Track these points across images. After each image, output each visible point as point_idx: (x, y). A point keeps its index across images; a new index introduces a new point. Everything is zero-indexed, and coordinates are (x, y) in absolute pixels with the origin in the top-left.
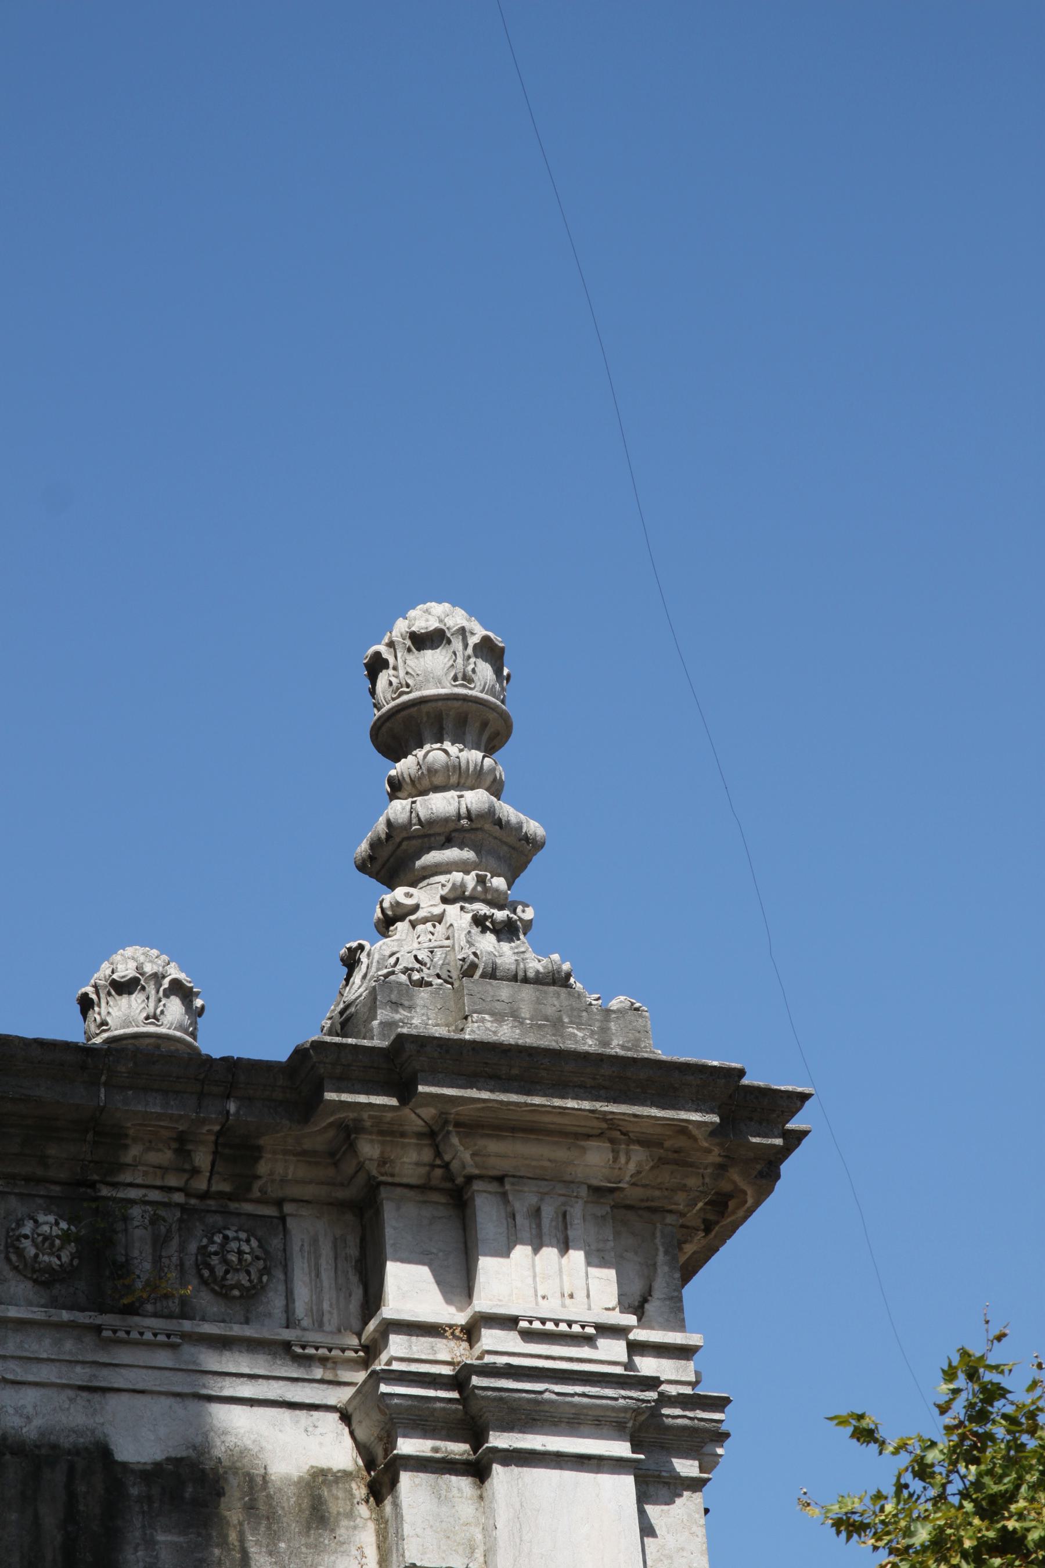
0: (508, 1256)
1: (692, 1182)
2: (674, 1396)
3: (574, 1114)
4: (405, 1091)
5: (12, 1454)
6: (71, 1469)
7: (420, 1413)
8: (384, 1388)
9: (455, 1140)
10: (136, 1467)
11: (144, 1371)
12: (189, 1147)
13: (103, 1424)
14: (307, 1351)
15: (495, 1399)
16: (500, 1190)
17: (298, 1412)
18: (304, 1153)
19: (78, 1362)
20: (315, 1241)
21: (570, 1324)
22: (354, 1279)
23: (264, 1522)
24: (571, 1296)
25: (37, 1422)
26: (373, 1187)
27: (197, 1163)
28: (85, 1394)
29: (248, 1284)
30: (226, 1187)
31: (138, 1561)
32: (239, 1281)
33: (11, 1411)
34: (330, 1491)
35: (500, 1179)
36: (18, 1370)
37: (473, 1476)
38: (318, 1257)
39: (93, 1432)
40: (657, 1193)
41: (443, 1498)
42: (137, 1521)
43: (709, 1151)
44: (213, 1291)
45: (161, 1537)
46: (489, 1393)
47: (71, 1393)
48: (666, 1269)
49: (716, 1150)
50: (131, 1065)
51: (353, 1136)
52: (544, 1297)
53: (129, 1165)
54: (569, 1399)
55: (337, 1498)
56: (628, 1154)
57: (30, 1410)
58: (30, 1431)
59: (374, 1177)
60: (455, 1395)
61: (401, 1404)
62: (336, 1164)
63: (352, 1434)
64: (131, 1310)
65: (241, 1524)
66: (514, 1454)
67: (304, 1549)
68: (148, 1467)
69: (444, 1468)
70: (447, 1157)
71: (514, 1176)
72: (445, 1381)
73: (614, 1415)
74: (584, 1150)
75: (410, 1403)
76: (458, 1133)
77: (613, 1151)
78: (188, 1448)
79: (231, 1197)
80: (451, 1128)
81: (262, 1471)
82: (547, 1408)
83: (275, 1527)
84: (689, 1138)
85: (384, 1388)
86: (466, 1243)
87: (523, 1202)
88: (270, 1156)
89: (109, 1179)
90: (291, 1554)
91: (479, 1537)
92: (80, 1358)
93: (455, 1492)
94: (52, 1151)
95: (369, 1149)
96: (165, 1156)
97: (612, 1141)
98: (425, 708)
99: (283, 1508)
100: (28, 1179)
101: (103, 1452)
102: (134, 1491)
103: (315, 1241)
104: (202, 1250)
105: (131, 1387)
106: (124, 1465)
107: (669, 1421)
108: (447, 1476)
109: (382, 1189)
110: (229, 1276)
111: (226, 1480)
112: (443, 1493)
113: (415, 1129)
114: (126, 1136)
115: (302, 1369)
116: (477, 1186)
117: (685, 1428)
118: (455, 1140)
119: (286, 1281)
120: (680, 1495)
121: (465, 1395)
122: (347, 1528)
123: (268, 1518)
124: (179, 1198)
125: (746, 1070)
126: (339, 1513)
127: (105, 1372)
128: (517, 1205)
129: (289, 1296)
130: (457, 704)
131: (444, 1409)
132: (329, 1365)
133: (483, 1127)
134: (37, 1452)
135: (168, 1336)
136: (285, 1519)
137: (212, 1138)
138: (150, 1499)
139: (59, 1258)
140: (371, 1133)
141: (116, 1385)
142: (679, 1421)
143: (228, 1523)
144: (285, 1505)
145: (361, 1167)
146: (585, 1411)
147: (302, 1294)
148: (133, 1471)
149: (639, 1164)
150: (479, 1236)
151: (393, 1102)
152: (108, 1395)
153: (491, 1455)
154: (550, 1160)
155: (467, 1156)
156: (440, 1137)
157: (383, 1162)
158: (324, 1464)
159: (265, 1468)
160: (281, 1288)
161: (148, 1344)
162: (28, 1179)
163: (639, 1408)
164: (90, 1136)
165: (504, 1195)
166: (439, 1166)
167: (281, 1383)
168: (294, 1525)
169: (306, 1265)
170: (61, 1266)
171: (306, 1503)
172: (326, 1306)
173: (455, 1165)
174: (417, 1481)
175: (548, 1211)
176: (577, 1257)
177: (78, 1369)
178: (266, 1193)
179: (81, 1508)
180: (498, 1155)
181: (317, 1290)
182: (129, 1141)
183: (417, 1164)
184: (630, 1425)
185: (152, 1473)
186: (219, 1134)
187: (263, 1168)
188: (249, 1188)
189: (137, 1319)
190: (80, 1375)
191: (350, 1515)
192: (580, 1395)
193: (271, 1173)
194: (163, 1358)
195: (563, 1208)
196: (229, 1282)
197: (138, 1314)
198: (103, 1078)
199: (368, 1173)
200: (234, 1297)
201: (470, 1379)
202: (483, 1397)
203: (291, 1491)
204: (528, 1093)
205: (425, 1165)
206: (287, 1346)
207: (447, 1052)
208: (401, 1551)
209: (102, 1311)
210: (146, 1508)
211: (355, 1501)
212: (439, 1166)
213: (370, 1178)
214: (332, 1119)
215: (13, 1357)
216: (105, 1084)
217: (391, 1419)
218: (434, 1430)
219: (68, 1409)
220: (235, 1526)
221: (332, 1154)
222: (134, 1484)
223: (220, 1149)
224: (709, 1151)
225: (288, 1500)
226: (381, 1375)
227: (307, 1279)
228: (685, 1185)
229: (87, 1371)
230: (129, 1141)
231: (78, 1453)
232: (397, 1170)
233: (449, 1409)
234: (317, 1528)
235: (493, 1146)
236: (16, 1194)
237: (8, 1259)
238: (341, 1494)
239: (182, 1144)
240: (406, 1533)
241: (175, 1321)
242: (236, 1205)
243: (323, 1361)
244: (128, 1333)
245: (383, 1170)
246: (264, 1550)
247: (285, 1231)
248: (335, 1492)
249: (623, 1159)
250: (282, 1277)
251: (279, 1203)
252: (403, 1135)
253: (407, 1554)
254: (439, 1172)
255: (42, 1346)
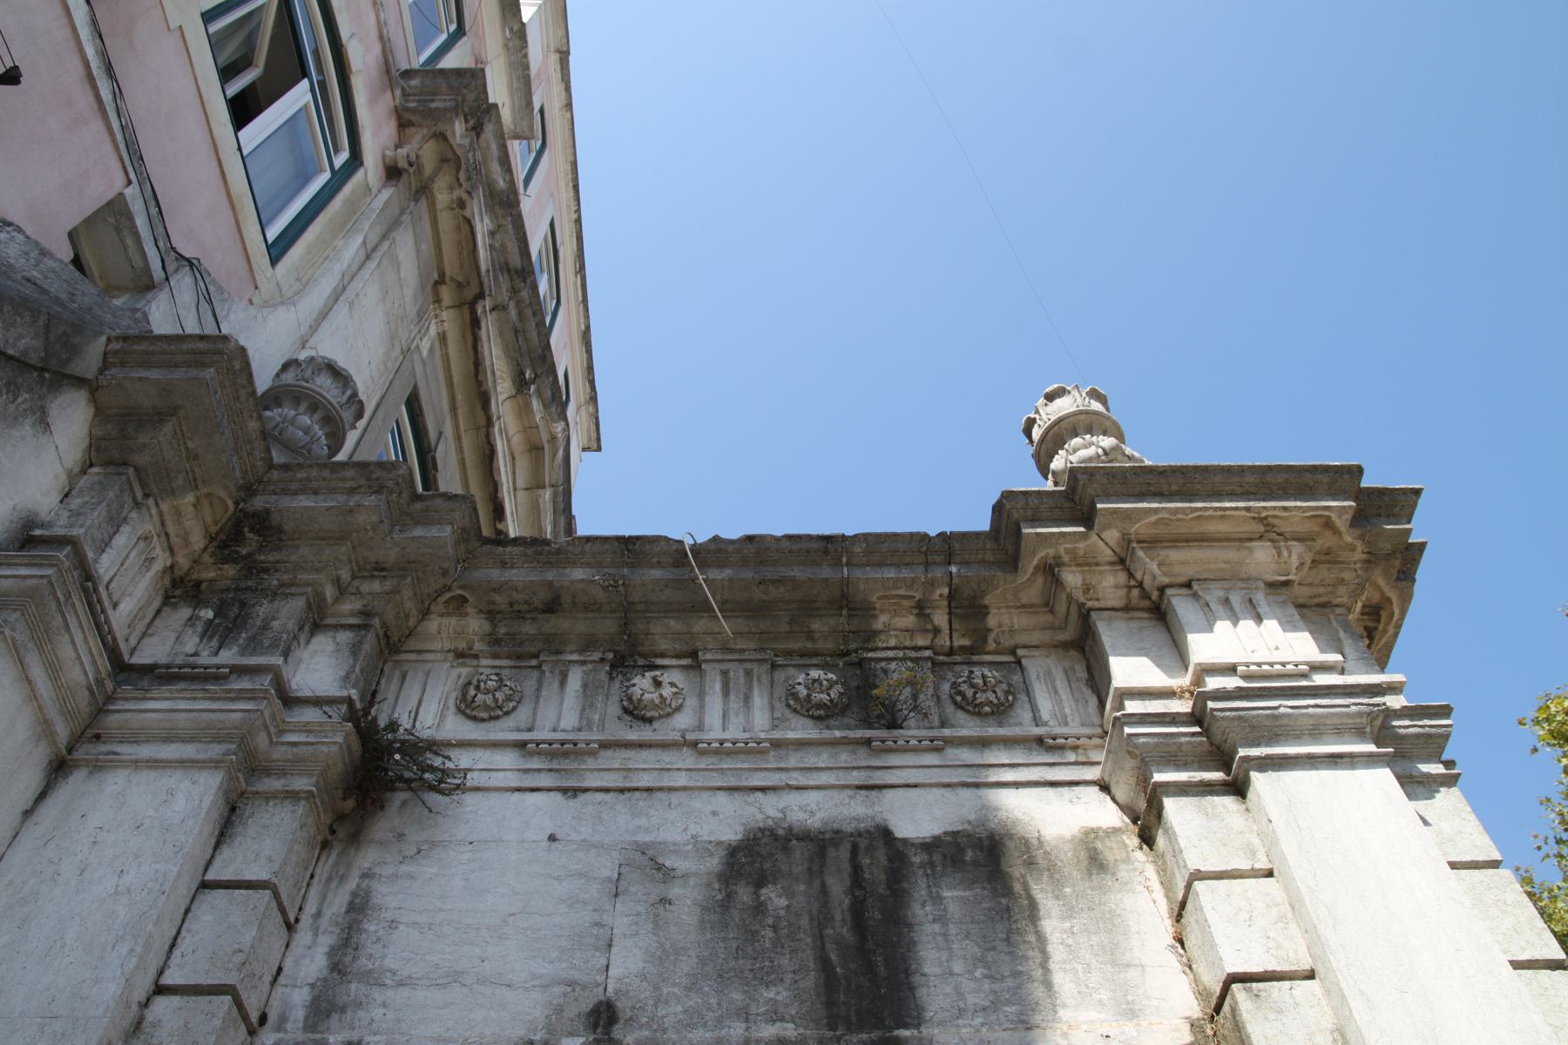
0: (1211, 631)
1: (1347, 575)
2: (1399, 710)
3: (1233, 516)
4: (1087, 518)
5: (798, 840)
6: (855, 849)
7: (1169, 749)
8: (1127, 730)
9: (1140, 553)
10: (916, 841)
11: (914, 770)
12: (927, 611)
13: (881, 812)
14: (1057, 741)
15: (1234, 718)
16: (1190, 592)
17: (1060, 789)
18: (1023, 606)
19: (854, 768)
20: (1049, 673)
21: (1283, 664)
22: (1088, 692)
23: (1046, 874)
24: (1277, 648)
25: (820, 815)
26: (1085, 616)
27: (936, 623)
28: (863, 792)
29: (995, 701)
30: (966, 642)
31: (927, 915)
32: (987, 698)
33: (796, 808)
34: (1103, 844)
35: (1188, 585)
36: (801, 778)
37: (1234, 795)
38: (1053, 681)
39: (873, 818)
40: (1322, 590)
41: (1210, 814)
42: (922, 882)
43: (1353, 549)
44: (968, 712)
45: (947, 894)
46: (1228, 714)
47: (850, 792)
48: (1350, 641)
49: (1360, 546)
50: (864, 545)
51: (1056, 569)
52: (1253, 652)
53: (881, 631)
54: (1304, 711)
55: (1112, 849)
56: (1288, 548)
57: (814, 807)
58: (815, 823)
59: (1083, 604)
60: (1197, 729)
61: (1148, 743)
62: (1051, 611)
63: (1113, 799)
64: (894, 725)
65: (1023, 876)
66: (1268, 761)
67: (1089, 892)
68: (928, 840)
69: (1203, 791)
70: (1139, 576)
71: (1198, 580)
72: (1185, 719)
73: (1351, 721)
74: (1251, 550)
75: (1156, 740)
76: (1141, 548)
77: (1275, 547)
78: (963, 824)
79: (972, 650)
80: (1134, 545)
81: (1037, 835)
82: (1285, 722)
83: (1058, 876)
84: (1335, 533)
85: (1127, 730)
86: (1174, 641)
87: (1213, 595)
88: (996, 611)
89: (866, 645)
90: (1077, 896)
91: (1256, 842)
92: (855, 764)
93: (1220, 809)
94: (816, 625)
95: (1072, 579)
96: (909, 621)
97: (1272, 541)
98: (1063, 424)
99: (1062, 861)
100: (802, 654)
101: (886, 833)
102: (917, 860)
103: (1049, 673)
104: (954, 685)
105: (904, 782)
106: (905, 841)
107: (1402, 731)
108: (1209, 797)
109: (1092, 613)
110: (978, 696)
111: (1003, 844)
112: (1210, 811)
113: (1106, 559)
114: (875, 609)
115: (1057, 756)
116: (1169, 592)
117: (1418, 736)
118: (1140, 553)
119: (1030, 701)
120: (1438, 791)
121: (1206, 725)
122: (1127, 871)
123: (1049, 870)
124: (927, 653)
125: (1363, 466)
126: (1116, 860)
127: (879, 773)
128: (1208, 598)
129: (1034, 709)
130: (1083, 417)
131: (1189, 742)
132: (1080, 751)
133: (1161, 541)
134: (821, 837)
135: (932, 741)
136: (1066, 870)
137: (946, 603)
138: (932, 865)
139: (829, 695)
140: (1071, 566)
141: (890, 782)
142: (1412, 730)
143: (1011, 877)
144: (1064, 858)
145: (1070, 597)
146: (1322, 720)
147: (1045, 706)
148: (913, 844)
149: (1300, 556)
150: (1183, 622)
151: (1082, 529)
152: (884, 791)
153: (1245, 765)
154: (1225, 562)
155: (1154, 567)
156: (1128, 560)
157: (1087, 589)
158: (1094, 824)
159: (1039, 832)
160: (1027, 706)
161: (915, 750)
162: (802, 654)
163: (1372, 712)
164: (845, 612)
165: (1195, 596)
166: (1134, 587)
167: (1040, 768)
168: (1075, 874)
169: (1044, 687)
170: (831, 701)
171: (1083, 854)
172: (1067, 711)
173: (1147, 583)
174: (1181, 803)
175: (1236, 599)
176: (1271, 625)
177: (855, 773)
178: (999, 643)
179: (867, 876)
180: (1181, 563)
181: (1057, 701)
182: (877, 612)
183: (1116, 587)
184: (1368, 729)
185: (930, 846)
186: (950, 597)
187: (992, 621)
188: (985, 641)
189: (901, 731)
190: (857, 777)
191: (1127, 860)
192: (1313, 706)
193: (1000, 626)
194: (930, 759)
195: (1248, 596)
196: (978, 701)
197: (902, 728)
198: (844, 560)
199: (1077, 601)
200: (987, 714)
201: (1206, 705)
202: (1222, 717)
203: (1067, 847)
204: (1190, 501)
205: (1122, 587)
206: (1040, 741)
207: (1114, 477)
208: (1182, 864)
209: (870, 727)
210: (929, 872)
211: (1130, 849)
212: (1134, 587)
213: (1081, 606)
214: (1035, 562)
215: (795, 769)
216: (847, 565)
217: (1143, 760)
218: (1186, 764)
219: (849, 804)
220: (1018, 879)
221: (1047, 605)
222: (916, 854)
223: (953, 610)
224: (1353, 549)
225: (1065, 853)
226: (1123, 720)
227: (1047, 695)
228: (1343, 579)
229: (863, 773)
230: (877, 612)
231: (860, 835)
232: (1100, 595)
233: (1194, 742)
234: (1098, 874)
235: (1174, 555)
236: (794, 666)
237: (788, 706)
238: (1114, 845)
239: (921, 609)
240: (1182, 845)
241: (935, 730)
242: (978, 657)
243: (1075, 748)
244: (895, 742)
245: (1088, 597)
246: (1050, 895)
247: (1022, 669)
248: (1108, 844)
249: (1285, 554)
250: (1026, 699)
251: (1013, 652)
252: (1097, 564)
253: (1189, 863)
254: (1136, 592)
255: (823, 758)
